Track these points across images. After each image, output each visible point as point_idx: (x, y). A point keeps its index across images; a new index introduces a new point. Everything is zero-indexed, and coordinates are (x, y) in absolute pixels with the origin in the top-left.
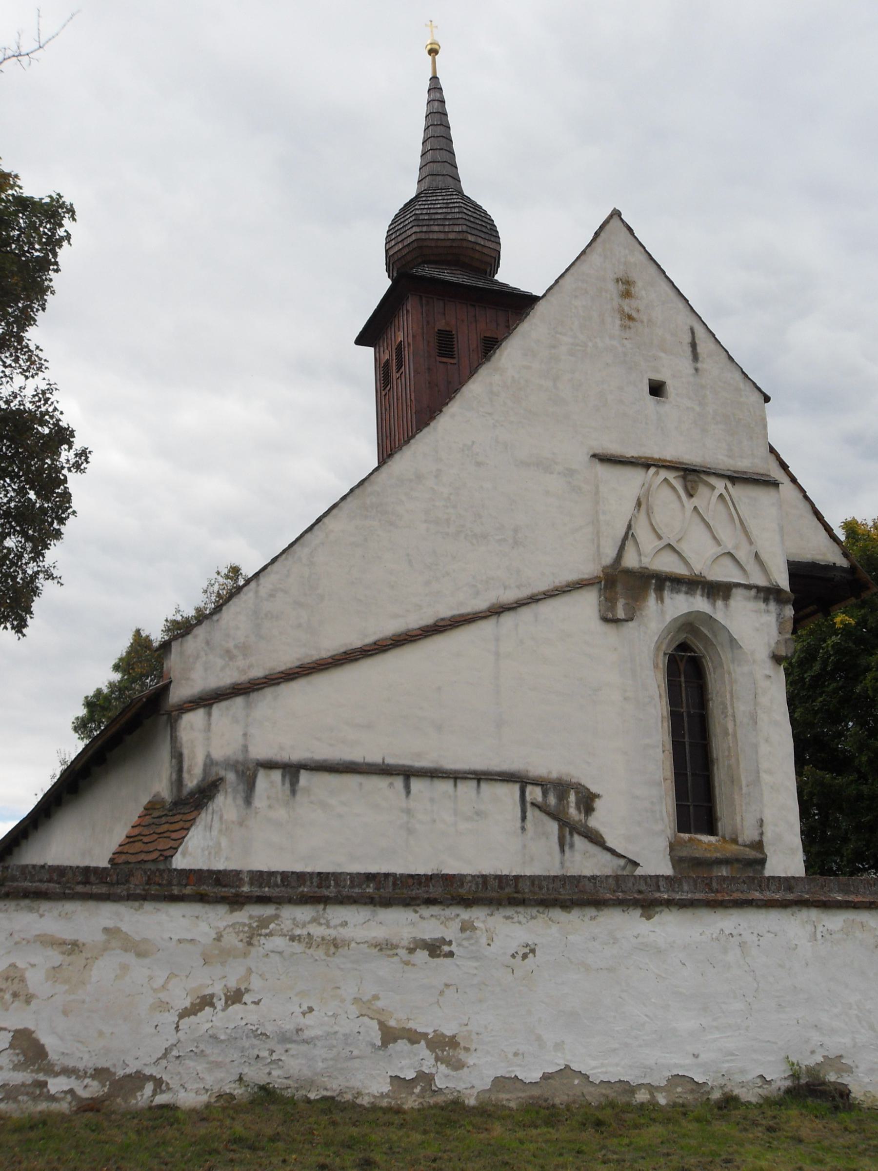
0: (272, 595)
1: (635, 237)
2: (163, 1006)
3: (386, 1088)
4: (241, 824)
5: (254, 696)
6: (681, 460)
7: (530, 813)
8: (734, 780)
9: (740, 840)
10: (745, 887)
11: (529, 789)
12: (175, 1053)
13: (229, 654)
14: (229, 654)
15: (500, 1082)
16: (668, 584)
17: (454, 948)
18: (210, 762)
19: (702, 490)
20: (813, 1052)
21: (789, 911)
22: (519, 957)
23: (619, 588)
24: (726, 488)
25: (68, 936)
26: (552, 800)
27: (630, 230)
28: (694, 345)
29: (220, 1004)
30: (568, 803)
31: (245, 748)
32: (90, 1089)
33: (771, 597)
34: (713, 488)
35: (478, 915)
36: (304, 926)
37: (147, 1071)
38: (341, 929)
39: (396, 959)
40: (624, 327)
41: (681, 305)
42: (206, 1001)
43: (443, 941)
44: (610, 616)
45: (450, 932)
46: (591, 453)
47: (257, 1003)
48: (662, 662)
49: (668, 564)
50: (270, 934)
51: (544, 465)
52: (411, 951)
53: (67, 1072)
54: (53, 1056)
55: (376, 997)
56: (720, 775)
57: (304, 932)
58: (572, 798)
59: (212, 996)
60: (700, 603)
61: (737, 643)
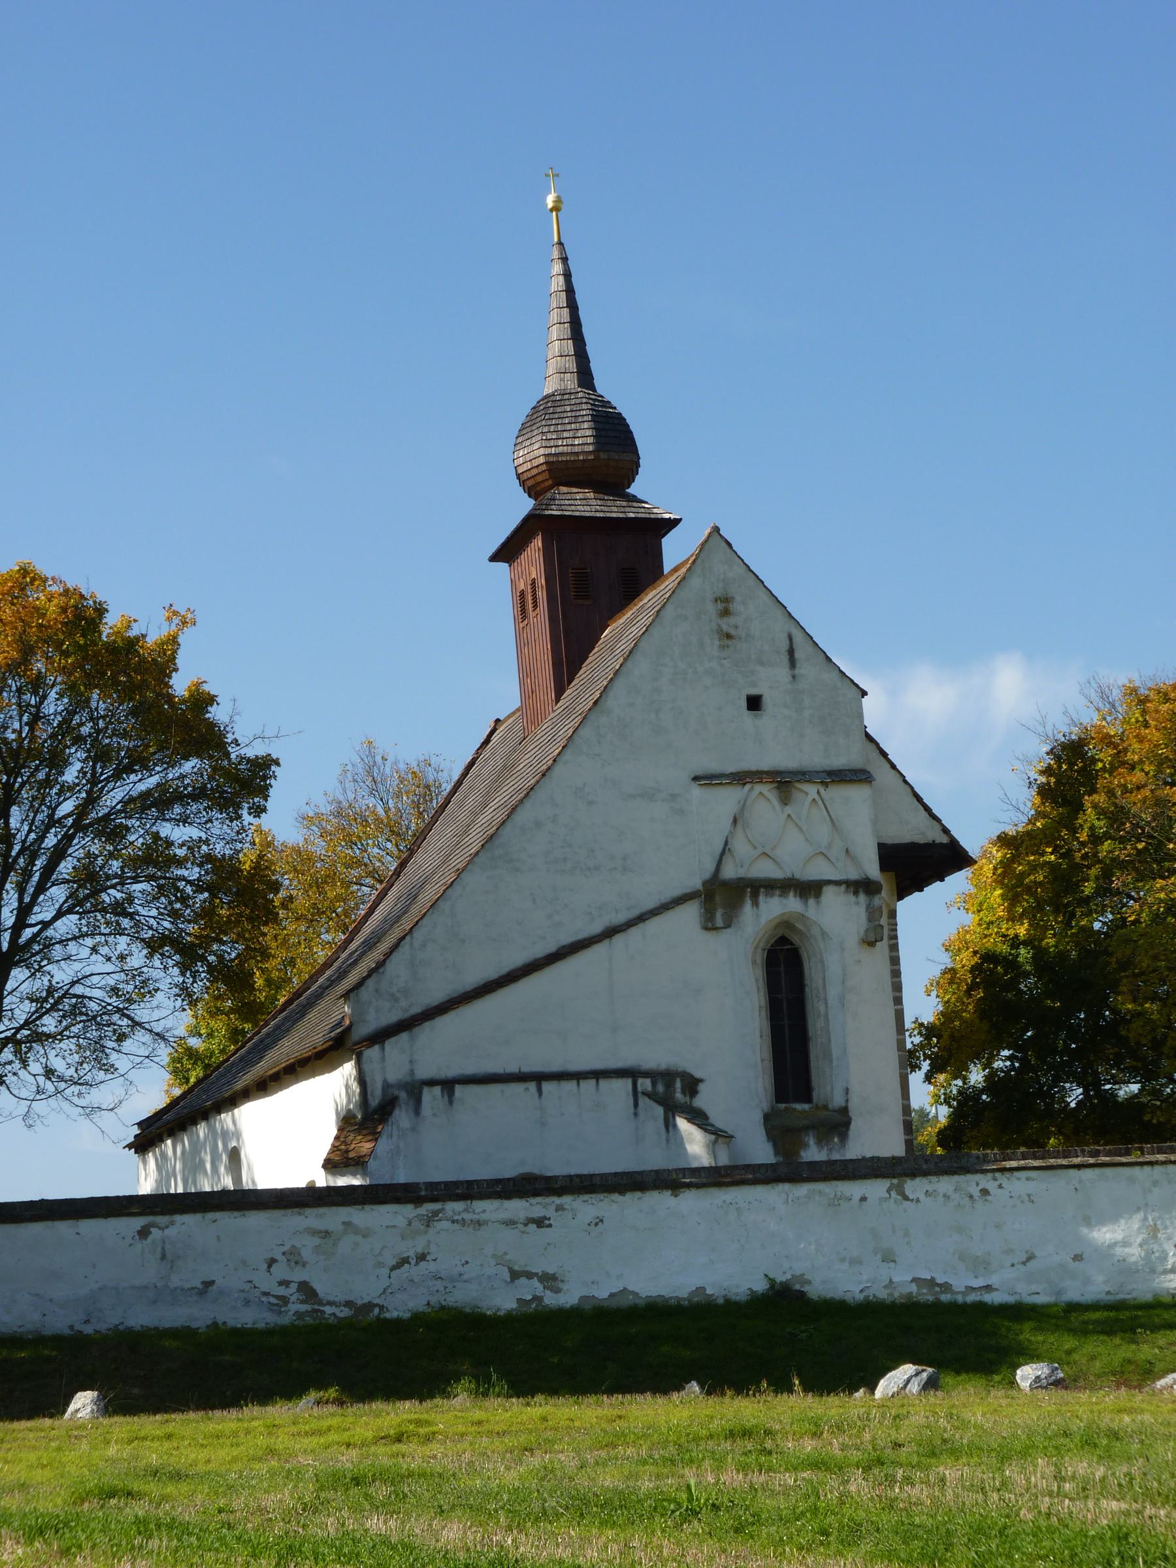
0: (424, 945)
1: (734, 551)
2: (380, 1265)
3: (514, 1305)
4: (414, 1129)
5: (416, 1030)
6: (778, 769)
7: (644, 1101)
8: (828, 1055)
9: (830, 1106)
10: (743, 1172)
11: (640, 1081)
12: (390, 1291)
13: (394, 998)
14: (394, 998)
15: (582, 1298)
16: (762, 890)
17: (551, 1222)
18: (386, 1085)
19: (796, 795)
20: (785, 1273)
21: (770, 1186)
22: (593, 1225)
23: (718, 899)
24: (818, 792)
25: (322, 1228)
26: (660, 1088)
27: (729, 545)
28: (791, 652)
29: (413, 1262)
30: (674, 1089)
31: (412, 1072)
32: (344, 1313)
33: (861, 890)
34: (807, 794)
35: (566, 1200)
36: (459, 1214)
37: (375, 1302)
38: (482, 1215)
39: (517, 1230)
40: (723, 647)
41: (779, 613)
42: (405, 1261)
43: (545, 1218)
44: (710, 925)
45: (550, 1212)
46: (692, 776)
47: (435, 1260)
48: (760, 958)
49: (765, 870)
50: (440, 1220)
51: (648, 795)
52: (526, 1225)
53: (330, 1303)
54: (321, 1295)
55: (506, 1253)
56: (814, 1051)
57: (459, 1218)
58: (678, 1085)
59: (408, 1257)
60: (792, 904)
61: (828, 935)
